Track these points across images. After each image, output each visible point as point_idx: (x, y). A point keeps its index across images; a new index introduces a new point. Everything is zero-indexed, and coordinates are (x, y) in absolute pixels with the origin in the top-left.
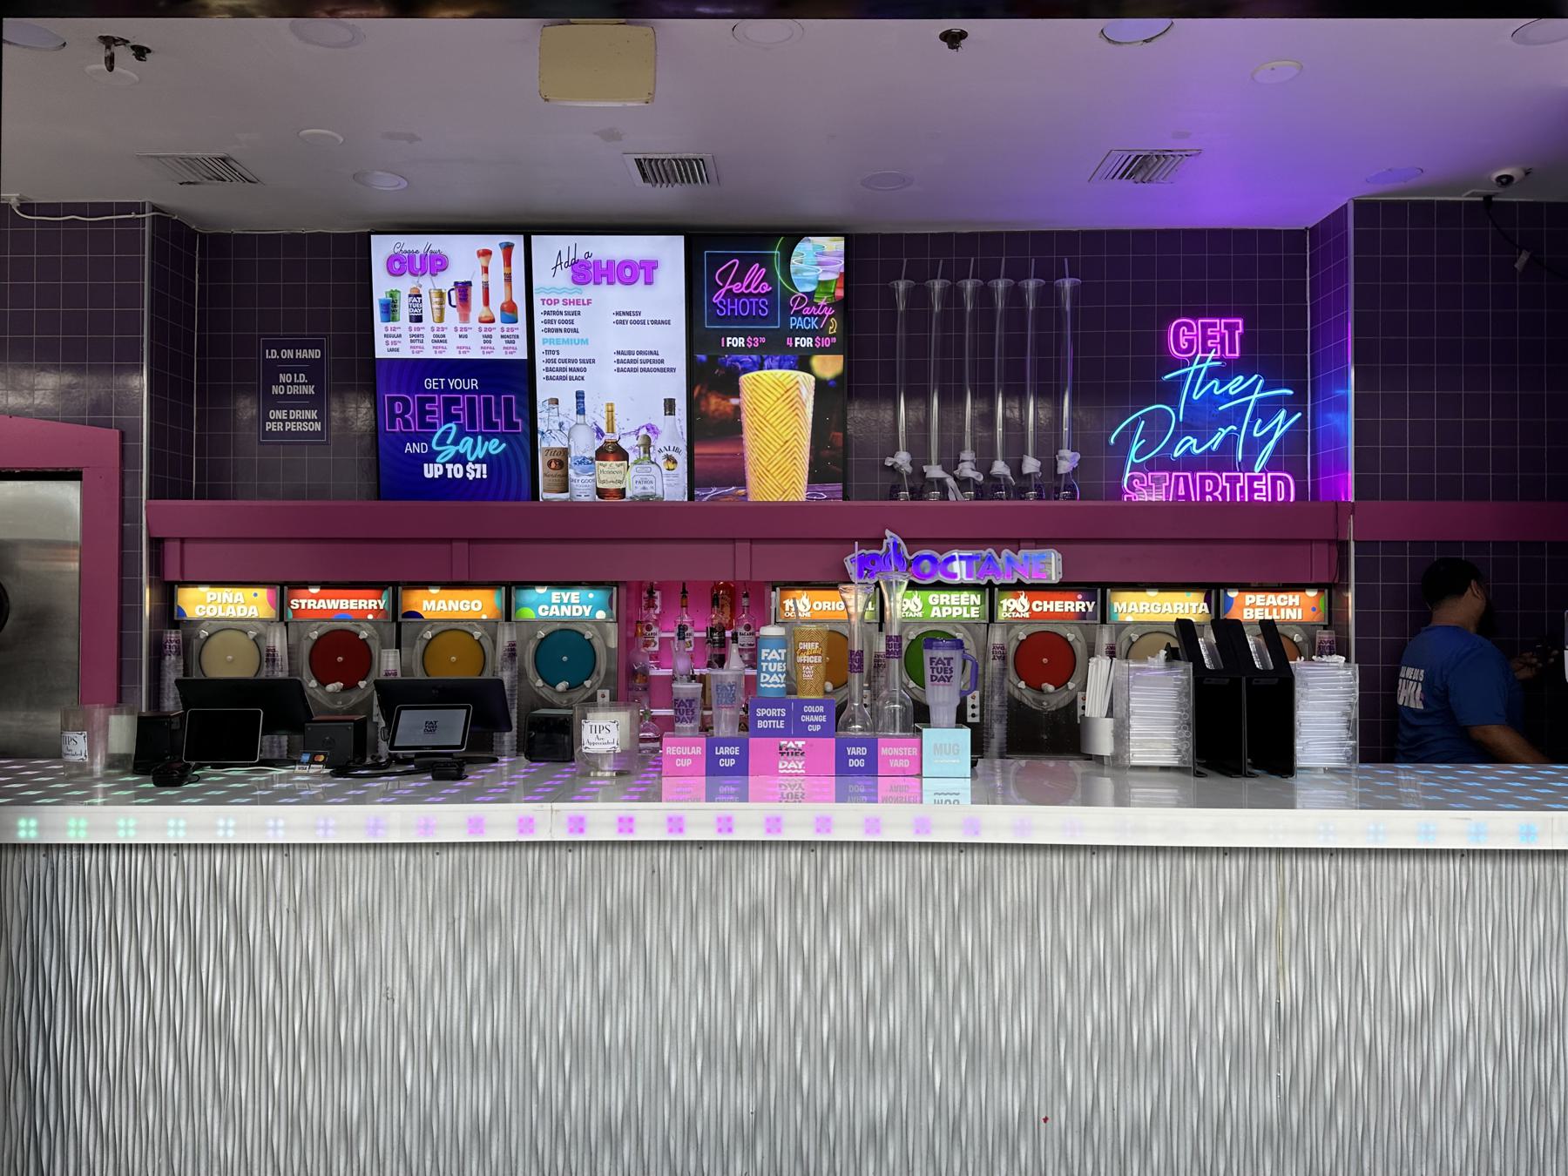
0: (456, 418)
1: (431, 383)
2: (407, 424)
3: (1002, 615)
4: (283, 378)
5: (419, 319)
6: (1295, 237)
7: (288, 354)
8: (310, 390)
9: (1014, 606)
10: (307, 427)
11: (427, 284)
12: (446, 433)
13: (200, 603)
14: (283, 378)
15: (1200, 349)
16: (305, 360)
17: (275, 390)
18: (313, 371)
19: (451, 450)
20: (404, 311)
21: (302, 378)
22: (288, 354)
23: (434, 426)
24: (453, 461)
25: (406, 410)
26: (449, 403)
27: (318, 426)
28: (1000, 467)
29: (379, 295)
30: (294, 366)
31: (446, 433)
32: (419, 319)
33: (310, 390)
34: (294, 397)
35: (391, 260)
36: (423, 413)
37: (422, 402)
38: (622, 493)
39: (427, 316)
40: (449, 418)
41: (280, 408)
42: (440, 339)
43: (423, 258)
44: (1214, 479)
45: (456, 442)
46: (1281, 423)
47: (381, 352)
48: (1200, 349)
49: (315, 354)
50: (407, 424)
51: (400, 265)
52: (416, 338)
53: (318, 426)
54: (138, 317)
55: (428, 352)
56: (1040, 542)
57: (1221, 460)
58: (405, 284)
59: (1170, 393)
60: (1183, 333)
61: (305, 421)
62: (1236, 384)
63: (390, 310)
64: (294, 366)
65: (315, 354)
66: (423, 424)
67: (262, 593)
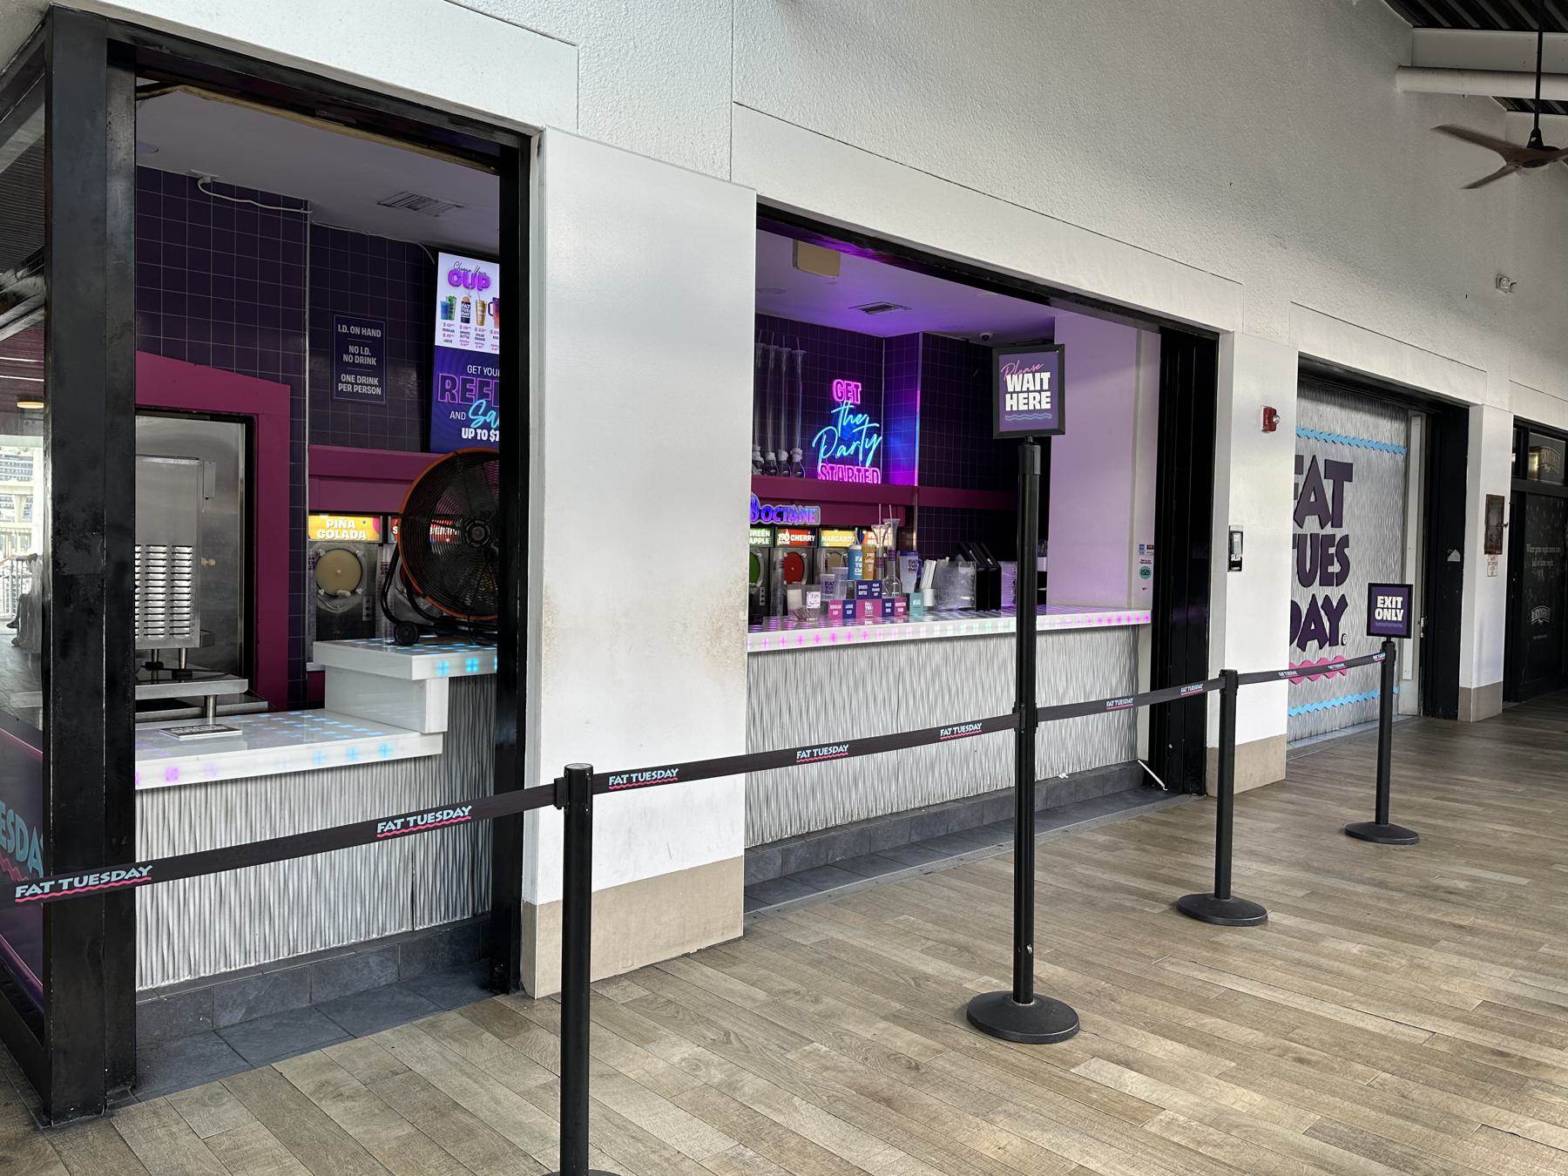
0: (486, 396)
1: (472, 369)
2: (453, 397)
3: (779, 543)
4: (351, 349)
5: (467, 321)
6: (879, 340)
7: (356, 330)
8: (373, 361)
9: (784, 538)
10: (371, 391)
11: (475, 296)
12: (479, 407)
13: (324, 528)
14: (351, 349)
15: (846, 394)
16: (369, 338)
17: (346, 358)
18: (374, 346)
19: (482, 419)
20: (458, 313)
21: (367, 351)
22: (356, 330)
23: (471, 400)
24: (481, 427)
25: (454, 387)
26: (483, 384)
27: (379, 391)
28: (772, 456)
29: (441, 298)
30: (361, 341)
31: (479, 407)
32: (467, 321)
33: (373, 361)
34: (360, 365)
35: (452, 274)
36: (465, 390)
37: (465, 381)
38: (1236, 565)
39: (473, 319)
40: (482, 396)
41: (350, 373)
42: (480, 338)
43: (474, 276)
44: (453, 380)
45: (485, 414)
46: (876, 441)
47: (439, 341)
48: (846, 394)
49: (376, 333)
50: (453, 397)
51: (457, 278)
52: (465, 334)
53: (379, 391)
54: (301, 294)
55: (472, 347)
56: (805, 502)
57: (852, 460)
58: (460, 293)
59: (833, 420)
60: (839, 387)
61: (369, 386)
62: (859, 418)
63: (448, 310)
64: (361, 341)
65: (376, 333)
66: (464, 398)
67: (369, 521)
